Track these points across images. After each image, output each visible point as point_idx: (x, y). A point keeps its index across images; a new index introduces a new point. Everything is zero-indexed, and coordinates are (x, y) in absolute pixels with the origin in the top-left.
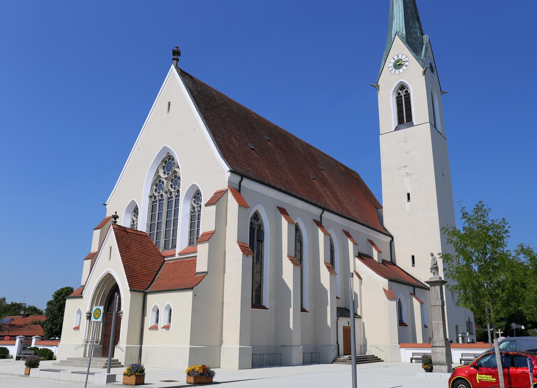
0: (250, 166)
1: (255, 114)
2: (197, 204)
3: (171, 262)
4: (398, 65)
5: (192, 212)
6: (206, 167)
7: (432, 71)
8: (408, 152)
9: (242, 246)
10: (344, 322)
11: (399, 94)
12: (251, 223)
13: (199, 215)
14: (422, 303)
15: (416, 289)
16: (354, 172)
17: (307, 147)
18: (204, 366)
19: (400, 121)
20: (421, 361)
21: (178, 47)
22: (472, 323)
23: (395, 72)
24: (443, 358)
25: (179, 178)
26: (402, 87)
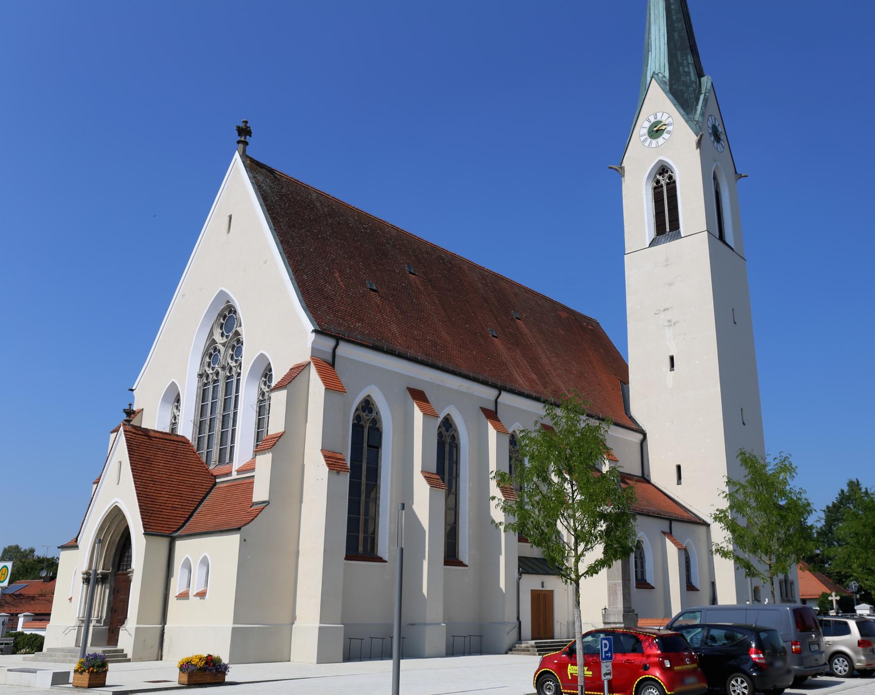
0: (361, 320)
1: (393, 227)
3: (225, 485)
4: (656, 131)
7: (718, 139)
8: (671, 285)
9: (330, 457)
10: (532, 582)
15: (674, 524)
16: (590, 319)
21: (246, 122)
26: (663, 169)
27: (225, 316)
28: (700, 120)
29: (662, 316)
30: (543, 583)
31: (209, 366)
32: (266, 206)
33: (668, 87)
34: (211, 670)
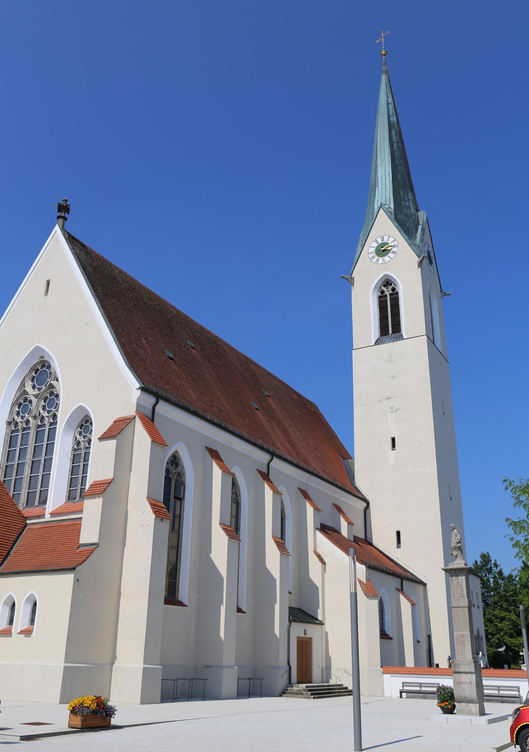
0: (168, 383)
1: (173, 307)
2: (85, 437)
4: (382, 251)
5: (76, 450)
6: (100, 378)
8: (393, 377)
9: (154, 505)
10: (298, 630)
11: (382, 292)
12: (167, 471)
13: (87, 454)
14: (413, 605)
15: (405, 582)
16: (311, 403)
17: (246, 361)
18: (98, 698)
19: (384, 331)
20: (435, 695)
21: (66, 201)
22: (482, 638)
23: (378, 260)
24: (471, 692)
25: (57, 396)
26: (387, 282)
27: (38, 370)
28: (420, 245)
29: (386, 403)
30: (305, 631)
31: (18, 414)
32: (86, 274)
33: (393, 216)
34: (101, 713)
